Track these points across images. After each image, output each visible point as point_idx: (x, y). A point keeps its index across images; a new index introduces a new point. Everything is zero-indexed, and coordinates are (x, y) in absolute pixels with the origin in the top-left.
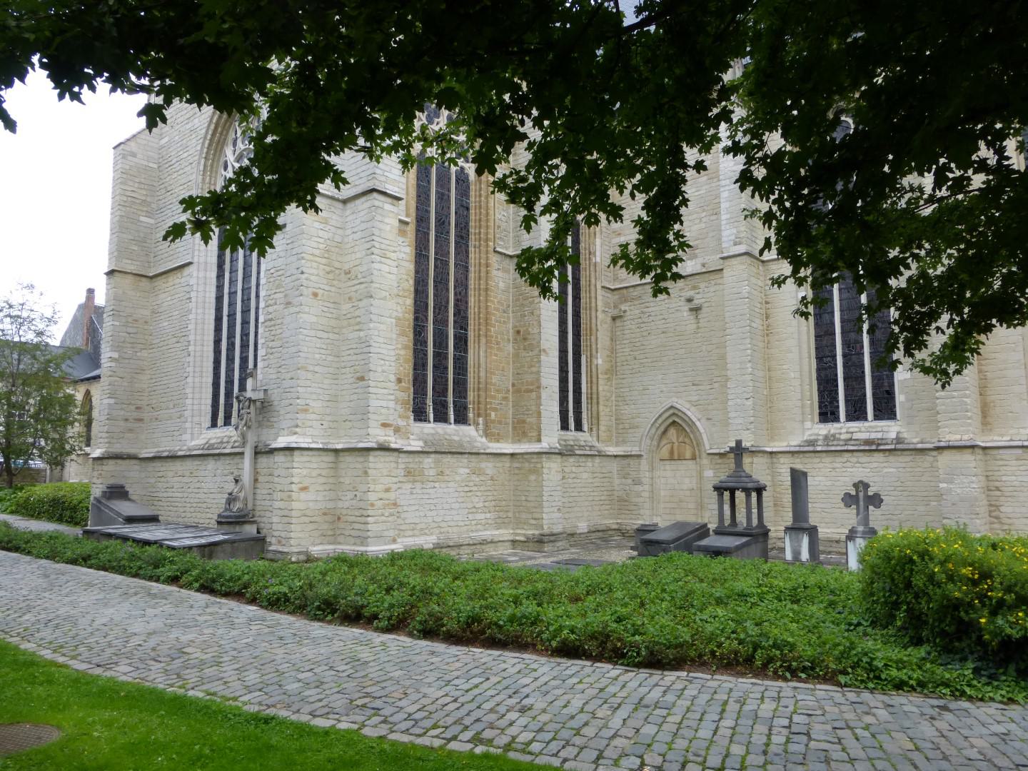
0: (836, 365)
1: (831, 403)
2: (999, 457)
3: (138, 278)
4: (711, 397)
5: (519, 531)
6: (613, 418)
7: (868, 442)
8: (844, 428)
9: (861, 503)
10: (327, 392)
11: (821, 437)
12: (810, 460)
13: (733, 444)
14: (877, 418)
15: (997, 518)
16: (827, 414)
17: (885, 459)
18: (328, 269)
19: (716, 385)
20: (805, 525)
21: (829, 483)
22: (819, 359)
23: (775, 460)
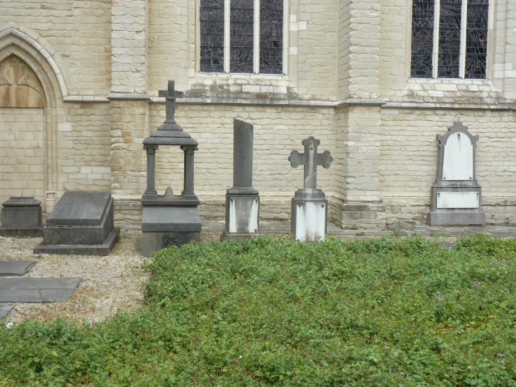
4: (70, 27)
7: (259, 96)
8: (228, 78)
9: (311, 162)
11: (207, 88)
12: (196, 114)
13: (165, 88)
14: (262, 70)
16: (420, 68)
19: (76, 12)
21: (218, 141)
23: (154, 112)
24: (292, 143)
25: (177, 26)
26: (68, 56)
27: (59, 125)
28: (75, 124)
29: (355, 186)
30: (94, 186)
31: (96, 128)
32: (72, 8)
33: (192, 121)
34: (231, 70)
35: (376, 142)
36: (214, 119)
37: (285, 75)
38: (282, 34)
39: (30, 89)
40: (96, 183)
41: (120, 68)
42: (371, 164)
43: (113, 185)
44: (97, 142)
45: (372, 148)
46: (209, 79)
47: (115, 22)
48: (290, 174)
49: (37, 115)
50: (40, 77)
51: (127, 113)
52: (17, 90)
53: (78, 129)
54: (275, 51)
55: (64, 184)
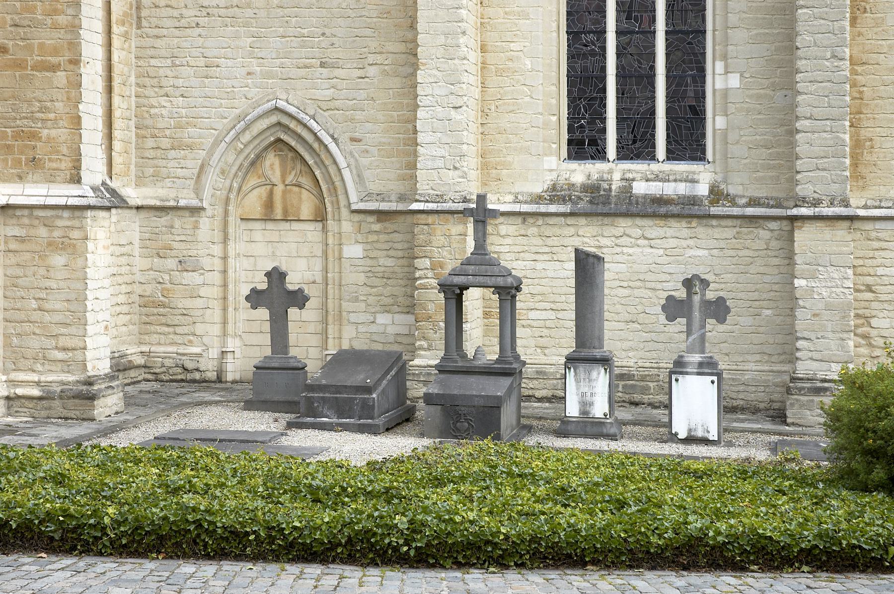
0: (604, 49)
1: (591, 122)
2: (874, 234)
4: (363, 94)
5: (21, 376)
6: (132, 124)
8: (612, 170)
9: (696, 314)
12: (557, 231)
15: (865, 337)
16: (584, 143)
17: (685, 232)
19: (372, 71)
20: (597, 353)
22: (573, 35)
24: (717, 280)
25: (525, 88)
26: (360, 141)
27: (345, 248)
28: (369, 247)
29: (810, 354)
30: (396, 345)
31: (400, 254)
32: (366, 66)
33: (549, 242)
34: (617, 155)
35: (845, 281)
36: (585, 240)
37: (709, 162)
38: (704, 92)
39: (303, 190)
40: (399, 339)
41: (430, 164)
42: (838, 318)
43: (418, 343)
44: (401, 276)
45: (838, 290)
46: (581, 172)
47: (422, 93)
48: (714, 332)
49: (312, 231)
50: (317, 173)
51: (439, 232)
52: (284, 192)
53: (373, 254)
54: (692, 123)
55: (350, 340)
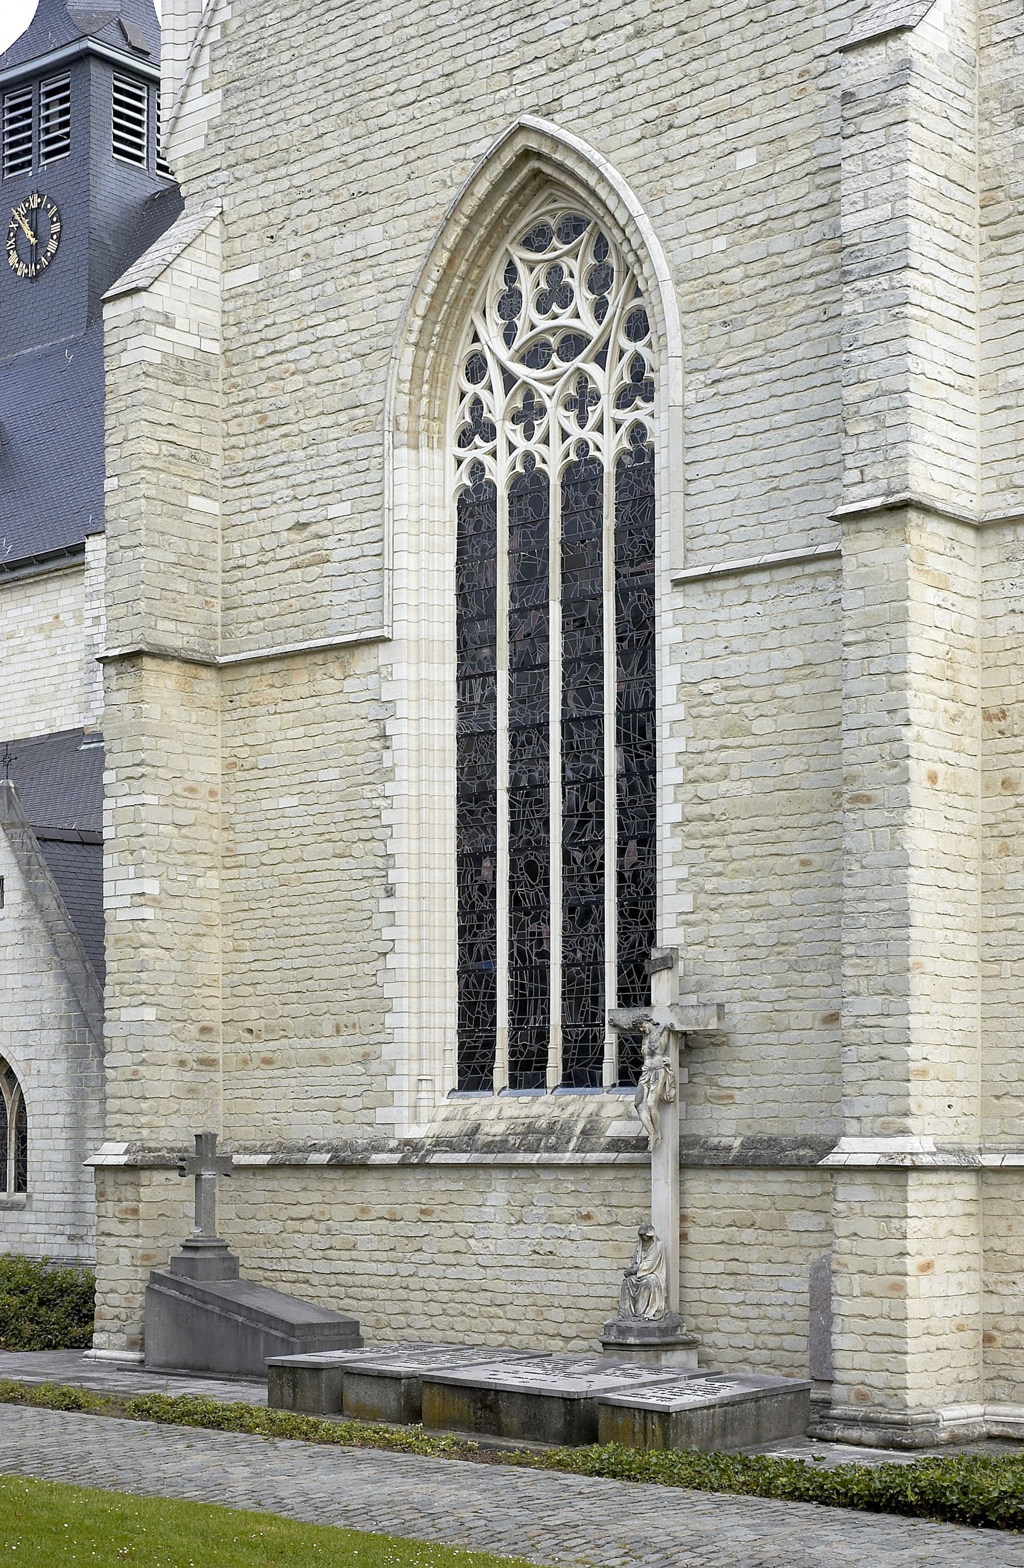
3: (192, 670)
8: (501, 1109)
10: (958, 1024)
18: (953, 708)
